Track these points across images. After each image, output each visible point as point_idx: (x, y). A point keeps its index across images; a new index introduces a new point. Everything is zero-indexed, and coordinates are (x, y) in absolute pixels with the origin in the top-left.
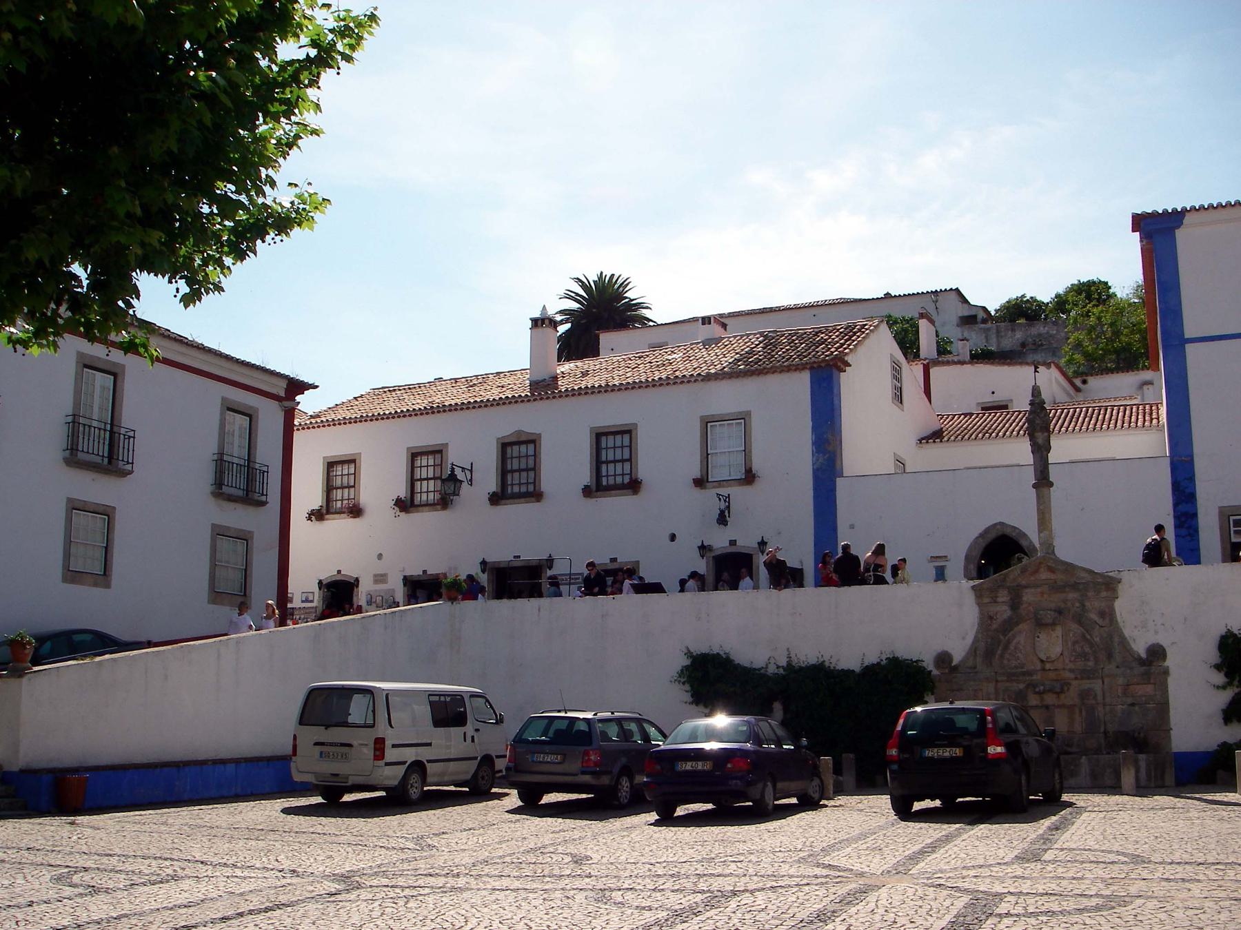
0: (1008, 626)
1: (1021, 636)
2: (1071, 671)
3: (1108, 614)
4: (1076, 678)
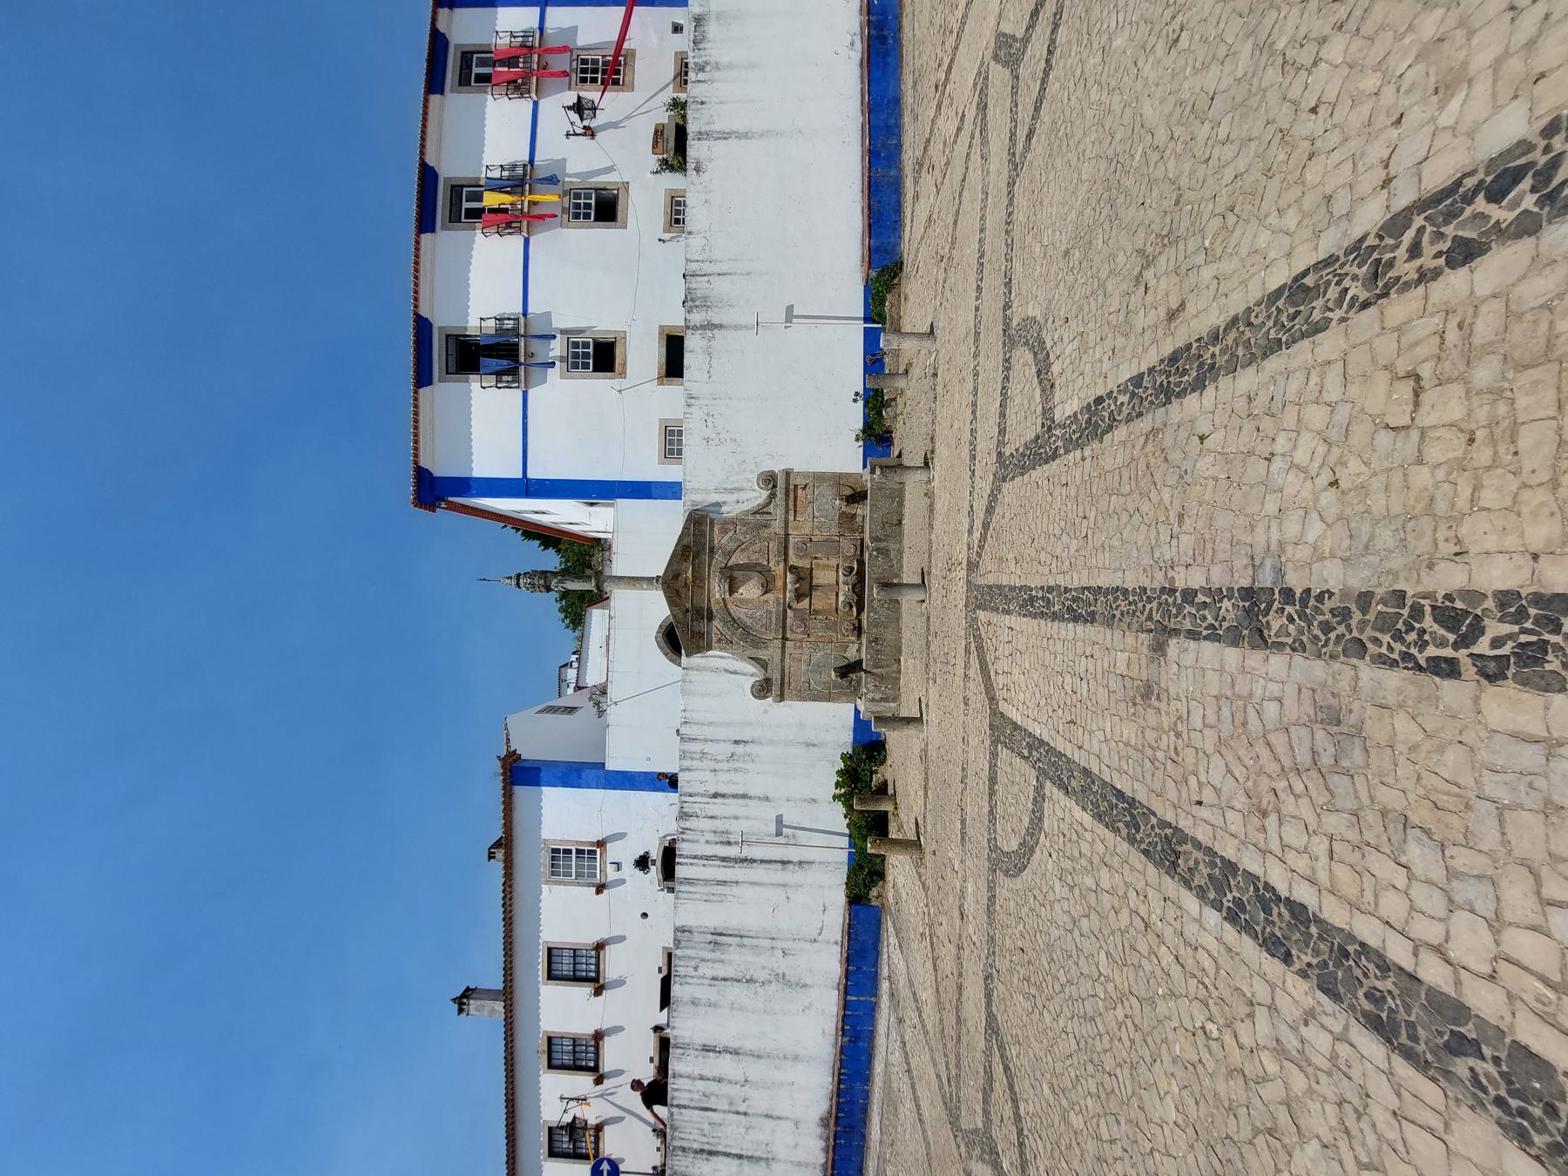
1: (739, 613)
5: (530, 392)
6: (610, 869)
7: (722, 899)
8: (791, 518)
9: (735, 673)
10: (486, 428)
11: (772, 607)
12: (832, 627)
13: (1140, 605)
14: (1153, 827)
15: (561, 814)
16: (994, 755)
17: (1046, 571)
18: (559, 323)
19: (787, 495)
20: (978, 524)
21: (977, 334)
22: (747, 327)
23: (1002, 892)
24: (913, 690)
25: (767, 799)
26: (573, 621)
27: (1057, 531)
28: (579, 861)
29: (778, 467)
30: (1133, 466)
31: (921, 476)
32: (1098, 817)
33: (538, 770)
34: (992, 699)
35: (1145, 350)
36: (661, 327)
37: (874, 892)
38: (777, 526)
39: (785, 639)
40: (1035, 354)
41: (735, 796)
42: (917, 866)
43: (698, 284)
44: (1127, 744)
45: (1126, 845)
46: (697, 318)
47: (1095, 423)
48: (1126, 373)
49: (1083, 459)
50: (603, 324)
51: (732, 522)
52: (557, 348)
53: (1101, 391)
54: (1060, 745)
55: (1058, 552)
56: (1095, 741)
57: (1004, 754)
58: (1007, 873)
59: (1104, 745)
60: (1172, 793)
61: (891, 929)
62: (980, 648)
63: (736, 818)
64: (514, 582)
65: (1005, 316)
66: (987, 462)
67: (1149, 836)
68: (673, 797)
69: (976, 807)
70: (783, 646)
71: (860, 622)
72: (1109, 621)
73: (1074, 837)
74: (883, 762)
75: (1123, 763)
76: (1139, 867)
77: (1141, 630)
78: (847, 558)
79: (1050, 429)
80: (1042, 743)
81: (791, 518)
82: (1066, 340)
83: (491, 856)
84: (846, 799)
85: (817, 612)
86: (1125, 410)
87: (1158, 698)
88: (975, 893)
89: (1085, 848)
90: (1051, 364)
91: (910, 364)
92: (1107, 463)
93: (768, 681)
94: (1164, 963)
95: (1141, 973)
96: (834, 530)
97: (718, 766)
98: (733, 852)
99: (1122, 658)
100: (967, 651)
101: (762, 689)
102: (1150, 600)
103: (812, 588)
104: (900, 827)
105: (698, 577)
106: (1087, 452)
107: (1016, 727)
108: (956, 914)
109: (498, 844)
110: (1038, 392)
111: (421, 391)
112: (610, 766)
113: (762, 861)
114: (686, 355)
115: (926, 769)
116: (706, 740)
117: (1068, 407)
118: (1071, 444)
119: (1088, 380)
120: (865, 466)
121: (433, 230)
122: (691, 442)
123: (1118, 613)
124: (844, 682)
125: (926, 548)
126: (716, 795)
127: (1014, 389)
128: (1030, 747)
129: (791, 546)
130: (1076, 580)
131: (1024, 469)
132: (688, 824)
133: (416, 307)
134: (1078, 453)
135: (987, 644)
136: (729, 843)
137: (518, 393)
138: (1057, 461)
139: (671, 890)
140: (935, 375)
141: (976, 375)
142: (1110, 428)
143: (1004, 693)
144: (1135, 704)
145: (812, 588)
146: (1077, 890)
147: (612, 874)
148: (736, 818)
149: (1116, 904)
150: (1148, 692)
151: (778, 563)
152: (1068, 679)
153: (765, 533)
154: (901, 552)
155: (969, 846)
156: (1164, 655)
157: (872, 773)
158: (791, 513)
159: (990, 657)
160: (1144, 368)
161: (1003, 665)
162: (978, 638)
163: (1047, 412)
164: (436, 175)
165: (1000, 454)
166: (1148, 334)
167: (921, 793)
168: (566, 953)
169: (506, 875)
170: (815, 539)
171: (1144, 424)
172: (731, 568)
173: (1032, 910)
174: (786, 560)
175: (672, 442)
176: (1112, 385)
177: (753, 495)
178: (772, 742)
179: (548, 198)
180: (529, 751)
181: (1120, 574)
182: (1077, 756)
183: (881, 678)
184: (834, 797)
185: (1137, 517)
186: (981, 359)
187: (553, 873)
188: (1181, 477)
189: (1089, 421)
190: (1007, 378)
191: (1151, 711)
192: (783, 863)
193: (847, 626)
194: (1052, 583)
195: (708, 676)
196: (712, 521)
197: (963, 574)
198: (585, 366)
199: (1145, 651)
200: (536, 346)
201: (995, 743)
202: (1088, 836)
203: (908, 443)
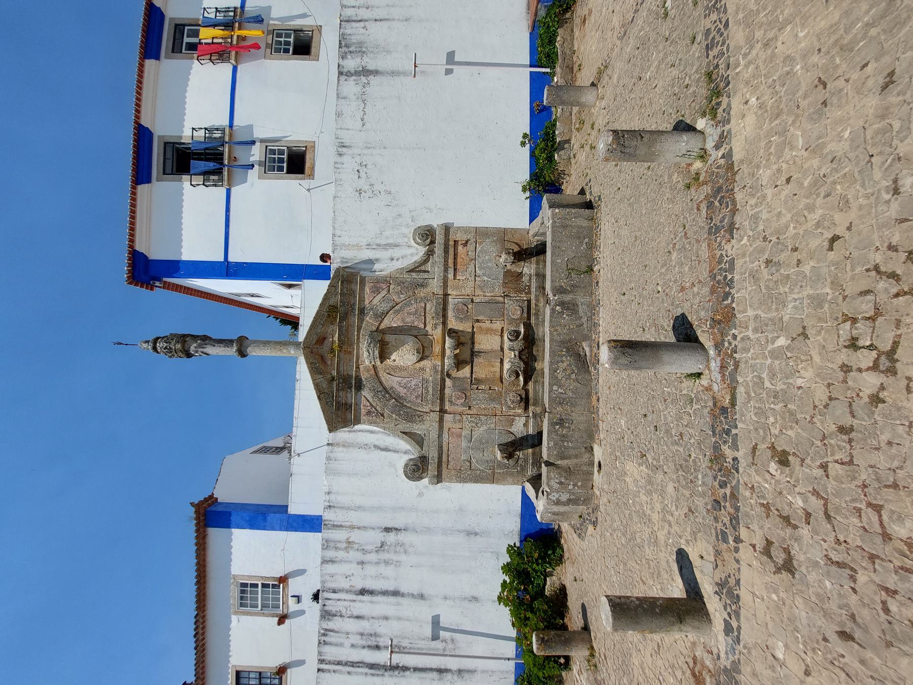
0: (385, 392)
1: (391, 381)
5: (233, 190)
6: (291, 601)
8: (451, 276)
9: (386, 449)
10: (193, 220)
11: (428, 375)
12: (497, 398)
15: (248, 553)
18: (258, 134)
19: (446, 251)
22: (405, 74)
25: (422, 597)
28: (266, 595)
29: (436, 222)
33: (229, 514)
38: (435, 286)
39: (442, 411)
41: (385, 593)
43: (356, 32)
50: (295, 134)
51: (386, 281)
52: (256, 154)
70: (441, 420)
71: (527, 392)
74: (560, 560)
78: (511, 321)
81: (451, 276)
85: (479, 381)
93: (423, 459)
96: (499, 291)
98: (382, 657)
101: (417, 469)
103: (473, 354)
105: (346, 343)
111: (139, 187)
112: (292, 510)
116: (352, 527)
121: (157, 58)
126: (363, 592)
129: (450, 307)
132: (330, 625)
133: (138, 117)
136: (378, 647)
145: (473, 354)
147: (293, 606)
151: (435, 326)
153: (421, 293)
154: (593, 308)
157: (546, 575)
158: (451, 271)
164: (162, 16)
168: (252, 675)
169: (198, 608)
170: (477, 300)
172: (383, 332)
174: (444, 323)
178: (428, 530)
179: (253, 33)
183: (569, 472)
187: (242, 605)
192: (440, 671)
193: (512, 397)
195: (361, 454)
196: (363, 280)
198: (280, 169)
200: (239, 152)
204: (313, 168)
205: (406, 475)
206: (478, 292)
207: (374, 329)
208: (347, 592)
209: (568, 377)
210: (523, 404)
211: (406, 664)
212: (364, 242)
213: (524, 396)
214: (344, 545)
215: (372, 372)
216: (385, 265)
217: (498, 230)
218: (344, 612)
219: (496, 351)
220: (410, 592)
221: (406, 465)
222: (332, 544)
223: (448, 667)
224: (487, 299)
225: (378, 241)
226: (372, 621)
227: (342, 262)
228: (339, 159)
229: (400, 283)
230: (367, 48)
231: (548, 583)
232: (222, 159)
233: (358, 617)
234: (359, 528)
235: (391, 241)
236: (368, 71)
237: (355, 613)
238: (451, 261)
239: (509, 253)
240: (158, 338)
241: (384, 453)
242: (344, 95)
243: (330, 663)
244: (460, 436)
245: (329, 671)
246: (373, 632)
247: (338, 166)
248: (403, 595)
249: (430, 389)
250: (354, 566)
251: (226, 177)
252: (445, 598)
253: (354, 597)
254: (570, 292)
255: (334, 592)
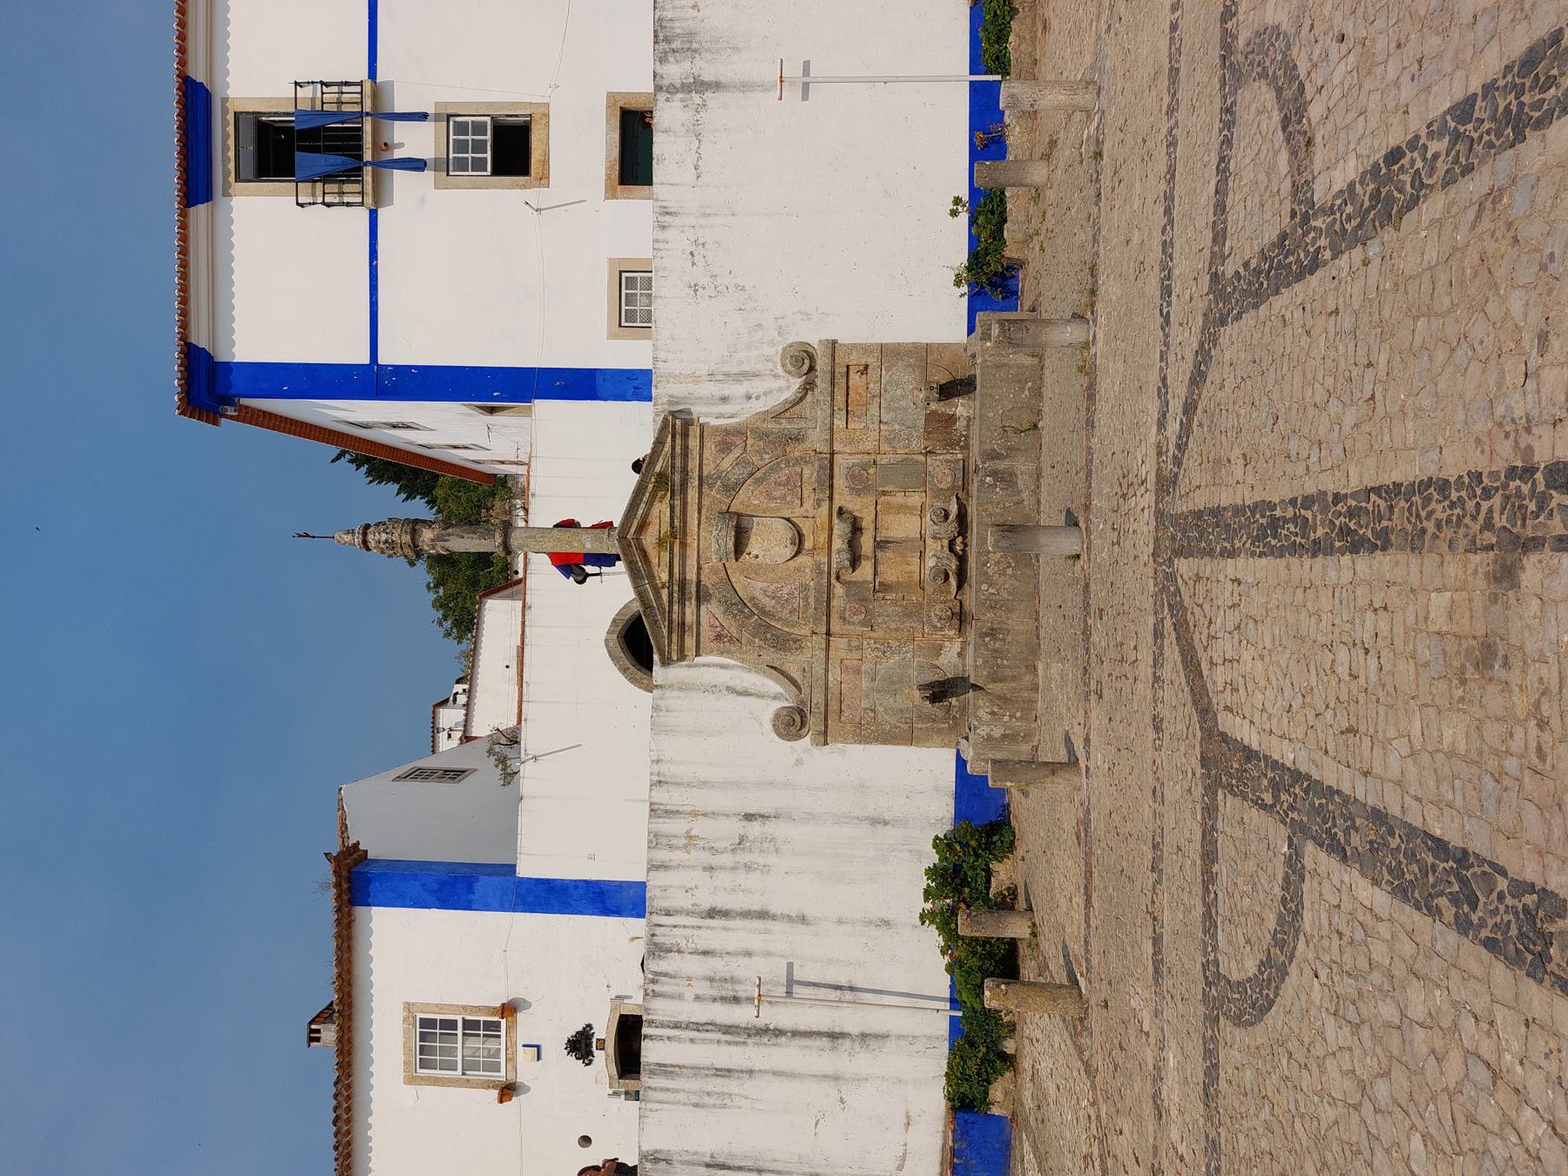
0: (737, 605)
1: (751, 587)
2: (818, 503)
3: (728, 439)
4: (831, 498)
7: (724, 1101)
8: (839, 423)
11: (808, 577)
13: (1470, 505)
14: (1501, 897)
16: (1210, 811)
17: (1301, 470)
20: (1176, 406)
21: (1174, 72)
22: (764, 87)
23: (1230, 1057)
24: (1060, 710)
25: (803, 919)
26: (457, 623)
27: (1319, 397)
29: (815, 336)
30: (1454, 263)
31: (1073, 333)
32: (1402, 892)
34: (1205, 712)
35: (1478, 53)
36: (612, 97)
37: (997, 1092)
40: (1279, 91)
41: (746, 914)
42: (1075, 1035)
44: (1451, 754)
45: (1452, 937)
46: (675, 71)
47: (1387, 195)
48: (1441, 103)
49: (1366, 263)
53: (1396, 138)
54: (1329, 774)
55: (1322, 432)
56: (1393, 759)
57: (1228, 805)
58: (1238, 1021)
59: (1408, 767)
60: (1534, 828)
61: (1029, 1157)
62: (1182, 628)
63: (749, 954)
64: (358, 540)
65: (1225, 32)
66: (1192, 294)
67: (1495, 912)
68: (636, 926)
69: (1179, 912)
72: (1416, 542)
73: (1359, 935)
75: (1445, 788)
76: (1477, 970)
77: (1473, 548)
78: (938, 493)
79: (1306, 218)
80: (1297, 776)
81: (839, 423)
82: (1334, 56)
83: (313, 1037)
84: (944, 921)
85: (886, 587)
86: (1442, 167)
87: (1506, 664)
88: (1180, 1067)
89: (1379, 952)
90: (1307, 104)
91: (1053, 143)
92: (1408, 263)
94: (1530, 1138)
95: (1487, 1164)
96: (918, 444)
97: (717, 860)
98: (742, 1015)
99: (1439, 602)
100: (1158, 634)
101: (792, 723)
102: (1487, 494)
104: (1043, 968)
105: (677, 535)
106: (1374, 249)
107: (1249, 754)
108: (1148, 1109)
109: (325, 1016)
110: (1284, 156)
112: (523, 871)
113: (796, 1034)
114: (658, 138)
115: (1089, 854)
116: (695, 814)
117: (1336, 173)
118: (1343, 241)
119: (1373, 123)
120: (971, 330)
122: (668, 302)
123: (1430, 526)
124: (936, 710)
125: (1081, 462)
126: (712, 913)
127: (1241, 158)
128: (1276, 787)
130: (1358, 476)
131: (1258, 298)
134: (1357, 254)
135: (1196, 616)
136: (736, 1000)
137: (363, 215)
138: (1319, 273)
139: (636, 1096)
140: (1098, 155)
141: (1172, 144)
142: (1414, 202)
143: (1227, 698)
144: (1463, 682)
146: (1365, 1032)
148: (749, 954)
149: (1438, 1044)
150: (1487, 656)
152: (1342, 654)
153: (796, 451)
155: (1167, 983)
156: (1516, 586)
159: (1199, 639)
160: (1475, 86)
161: (1225, 646)
162: (1177, 609)
163: (1301, 189)
165: (1215, 277)
166: (1484, 21)
167: (1079, 900)
171: (1474, 187)
173: (1285, 1079)
175: (632, 298)
176: (1416, 124)
177: (781, 383)
178: (810, 817)
180: (378, 846)
181: (1434, 455)
182: (1363, 791)
183: (1004, 700)
184: (922, 917)
185: (1462, 352)
186: (1181, 115)
187: (424, 1064)
188: (1543, 267)
189: (1376, 195)
190: (1227, 142)
191: (1492, 689)
192: (834, 1036)
194: (1311, 489)
197: (1148, 499)
198: (479, 165)
199: (1481, 583)
201: (1210, 791)
202: (1383, 930)
203: (1047, 281)
204: (546, 162)
205: (779, 735)
206: (885, 447)
207: (725, 508)
208: (689, 913)
209: (1003, 573)
210: (956, 622)
211: (781, 1026)
212: (704, 370)
213: (957, 610)
214: (683, 841)
215: (723, 574)
216: (738, 407)
217: (916, 346)
218: (683, 944)
219: (913, 540)
220: (786, 912)
221: (777, 716)
222: (664, 841)
223: (846, 1030)
224: (898, 458)
225: (726, 368)
226: (727, 958)
227: (670, 403)
228: (660, 235)
229: (762, 435)
230: (700, 42)
231: (993, 885)
232: (360, 148)
233: (705, 953)
234: (705, 815)
235: (747, 368)
236: (703, 83)
237: (701, 948)
238: (840, 398)
239: (932, 388)
240: (367, 527)
241: (741, 698)
242: (666, 125)
243: (662, 1025)
244: (858, 671)
245: (661, 1038)
246: (728, 976)
247: (660, 246)
248: (774, 918)
249: (811, 600)
250: (699, 873)
251: (369, 188)
252: (840, 922)
253: (698, 922)
254: (1005, 457)
255: (668, 914)
